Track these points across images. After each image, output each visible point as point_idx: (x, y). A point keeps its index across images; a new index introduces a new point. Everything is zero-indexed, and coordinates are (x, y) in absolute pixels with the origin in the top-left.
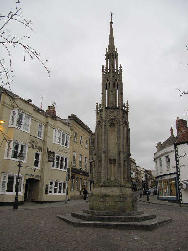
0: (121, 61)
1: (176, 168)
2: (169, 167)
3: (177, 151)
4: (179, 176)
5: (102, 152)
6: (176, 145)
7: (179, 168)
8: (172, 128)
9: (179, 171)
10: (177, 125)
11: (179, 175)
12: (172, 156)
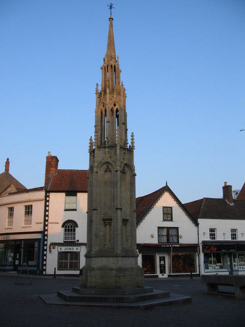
0: (125, 78)
1: (42, 225)
2: (28, 222)
3: (48, 201)
4: (46, 238)
5: (93, 210)
6: (48, 192)
7: (47, 225)
8: (8, 159)
9: (47, 230)
10: (47, 162)
11: (47, 235)
12: (38, 209)
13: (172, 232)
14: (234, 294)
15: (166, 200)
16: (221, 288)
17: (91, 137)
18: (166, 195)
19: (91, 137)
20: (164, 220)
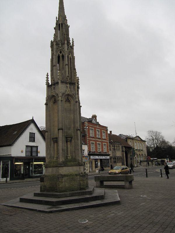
13: (34, 149)
14: (124, 186)
15: (31, 129)
16: (105, 183)
17: (48, 74)
18: (32, 126)
19: (48, 74)
20: (30, 141)
